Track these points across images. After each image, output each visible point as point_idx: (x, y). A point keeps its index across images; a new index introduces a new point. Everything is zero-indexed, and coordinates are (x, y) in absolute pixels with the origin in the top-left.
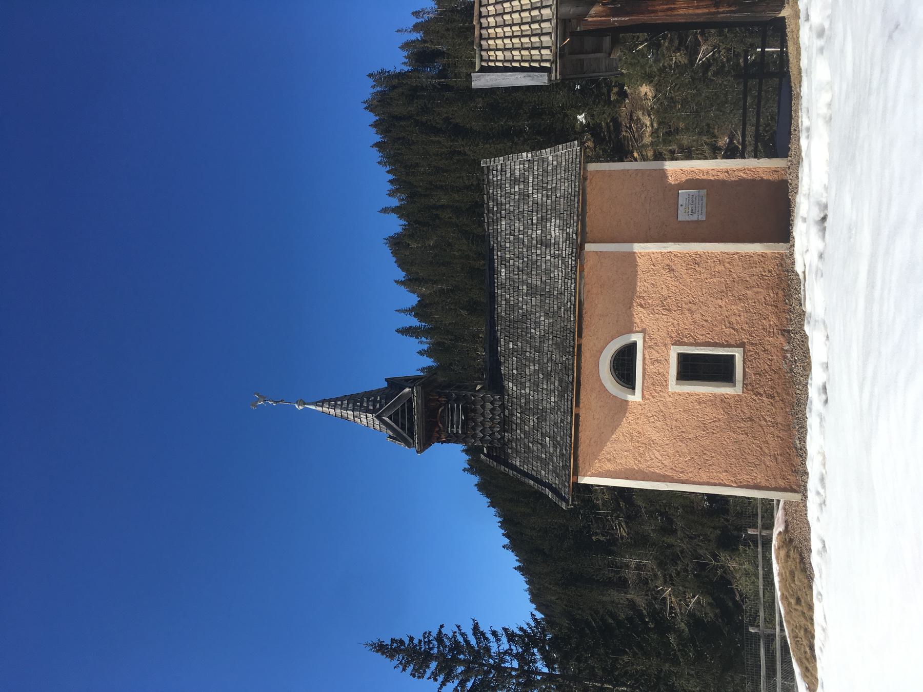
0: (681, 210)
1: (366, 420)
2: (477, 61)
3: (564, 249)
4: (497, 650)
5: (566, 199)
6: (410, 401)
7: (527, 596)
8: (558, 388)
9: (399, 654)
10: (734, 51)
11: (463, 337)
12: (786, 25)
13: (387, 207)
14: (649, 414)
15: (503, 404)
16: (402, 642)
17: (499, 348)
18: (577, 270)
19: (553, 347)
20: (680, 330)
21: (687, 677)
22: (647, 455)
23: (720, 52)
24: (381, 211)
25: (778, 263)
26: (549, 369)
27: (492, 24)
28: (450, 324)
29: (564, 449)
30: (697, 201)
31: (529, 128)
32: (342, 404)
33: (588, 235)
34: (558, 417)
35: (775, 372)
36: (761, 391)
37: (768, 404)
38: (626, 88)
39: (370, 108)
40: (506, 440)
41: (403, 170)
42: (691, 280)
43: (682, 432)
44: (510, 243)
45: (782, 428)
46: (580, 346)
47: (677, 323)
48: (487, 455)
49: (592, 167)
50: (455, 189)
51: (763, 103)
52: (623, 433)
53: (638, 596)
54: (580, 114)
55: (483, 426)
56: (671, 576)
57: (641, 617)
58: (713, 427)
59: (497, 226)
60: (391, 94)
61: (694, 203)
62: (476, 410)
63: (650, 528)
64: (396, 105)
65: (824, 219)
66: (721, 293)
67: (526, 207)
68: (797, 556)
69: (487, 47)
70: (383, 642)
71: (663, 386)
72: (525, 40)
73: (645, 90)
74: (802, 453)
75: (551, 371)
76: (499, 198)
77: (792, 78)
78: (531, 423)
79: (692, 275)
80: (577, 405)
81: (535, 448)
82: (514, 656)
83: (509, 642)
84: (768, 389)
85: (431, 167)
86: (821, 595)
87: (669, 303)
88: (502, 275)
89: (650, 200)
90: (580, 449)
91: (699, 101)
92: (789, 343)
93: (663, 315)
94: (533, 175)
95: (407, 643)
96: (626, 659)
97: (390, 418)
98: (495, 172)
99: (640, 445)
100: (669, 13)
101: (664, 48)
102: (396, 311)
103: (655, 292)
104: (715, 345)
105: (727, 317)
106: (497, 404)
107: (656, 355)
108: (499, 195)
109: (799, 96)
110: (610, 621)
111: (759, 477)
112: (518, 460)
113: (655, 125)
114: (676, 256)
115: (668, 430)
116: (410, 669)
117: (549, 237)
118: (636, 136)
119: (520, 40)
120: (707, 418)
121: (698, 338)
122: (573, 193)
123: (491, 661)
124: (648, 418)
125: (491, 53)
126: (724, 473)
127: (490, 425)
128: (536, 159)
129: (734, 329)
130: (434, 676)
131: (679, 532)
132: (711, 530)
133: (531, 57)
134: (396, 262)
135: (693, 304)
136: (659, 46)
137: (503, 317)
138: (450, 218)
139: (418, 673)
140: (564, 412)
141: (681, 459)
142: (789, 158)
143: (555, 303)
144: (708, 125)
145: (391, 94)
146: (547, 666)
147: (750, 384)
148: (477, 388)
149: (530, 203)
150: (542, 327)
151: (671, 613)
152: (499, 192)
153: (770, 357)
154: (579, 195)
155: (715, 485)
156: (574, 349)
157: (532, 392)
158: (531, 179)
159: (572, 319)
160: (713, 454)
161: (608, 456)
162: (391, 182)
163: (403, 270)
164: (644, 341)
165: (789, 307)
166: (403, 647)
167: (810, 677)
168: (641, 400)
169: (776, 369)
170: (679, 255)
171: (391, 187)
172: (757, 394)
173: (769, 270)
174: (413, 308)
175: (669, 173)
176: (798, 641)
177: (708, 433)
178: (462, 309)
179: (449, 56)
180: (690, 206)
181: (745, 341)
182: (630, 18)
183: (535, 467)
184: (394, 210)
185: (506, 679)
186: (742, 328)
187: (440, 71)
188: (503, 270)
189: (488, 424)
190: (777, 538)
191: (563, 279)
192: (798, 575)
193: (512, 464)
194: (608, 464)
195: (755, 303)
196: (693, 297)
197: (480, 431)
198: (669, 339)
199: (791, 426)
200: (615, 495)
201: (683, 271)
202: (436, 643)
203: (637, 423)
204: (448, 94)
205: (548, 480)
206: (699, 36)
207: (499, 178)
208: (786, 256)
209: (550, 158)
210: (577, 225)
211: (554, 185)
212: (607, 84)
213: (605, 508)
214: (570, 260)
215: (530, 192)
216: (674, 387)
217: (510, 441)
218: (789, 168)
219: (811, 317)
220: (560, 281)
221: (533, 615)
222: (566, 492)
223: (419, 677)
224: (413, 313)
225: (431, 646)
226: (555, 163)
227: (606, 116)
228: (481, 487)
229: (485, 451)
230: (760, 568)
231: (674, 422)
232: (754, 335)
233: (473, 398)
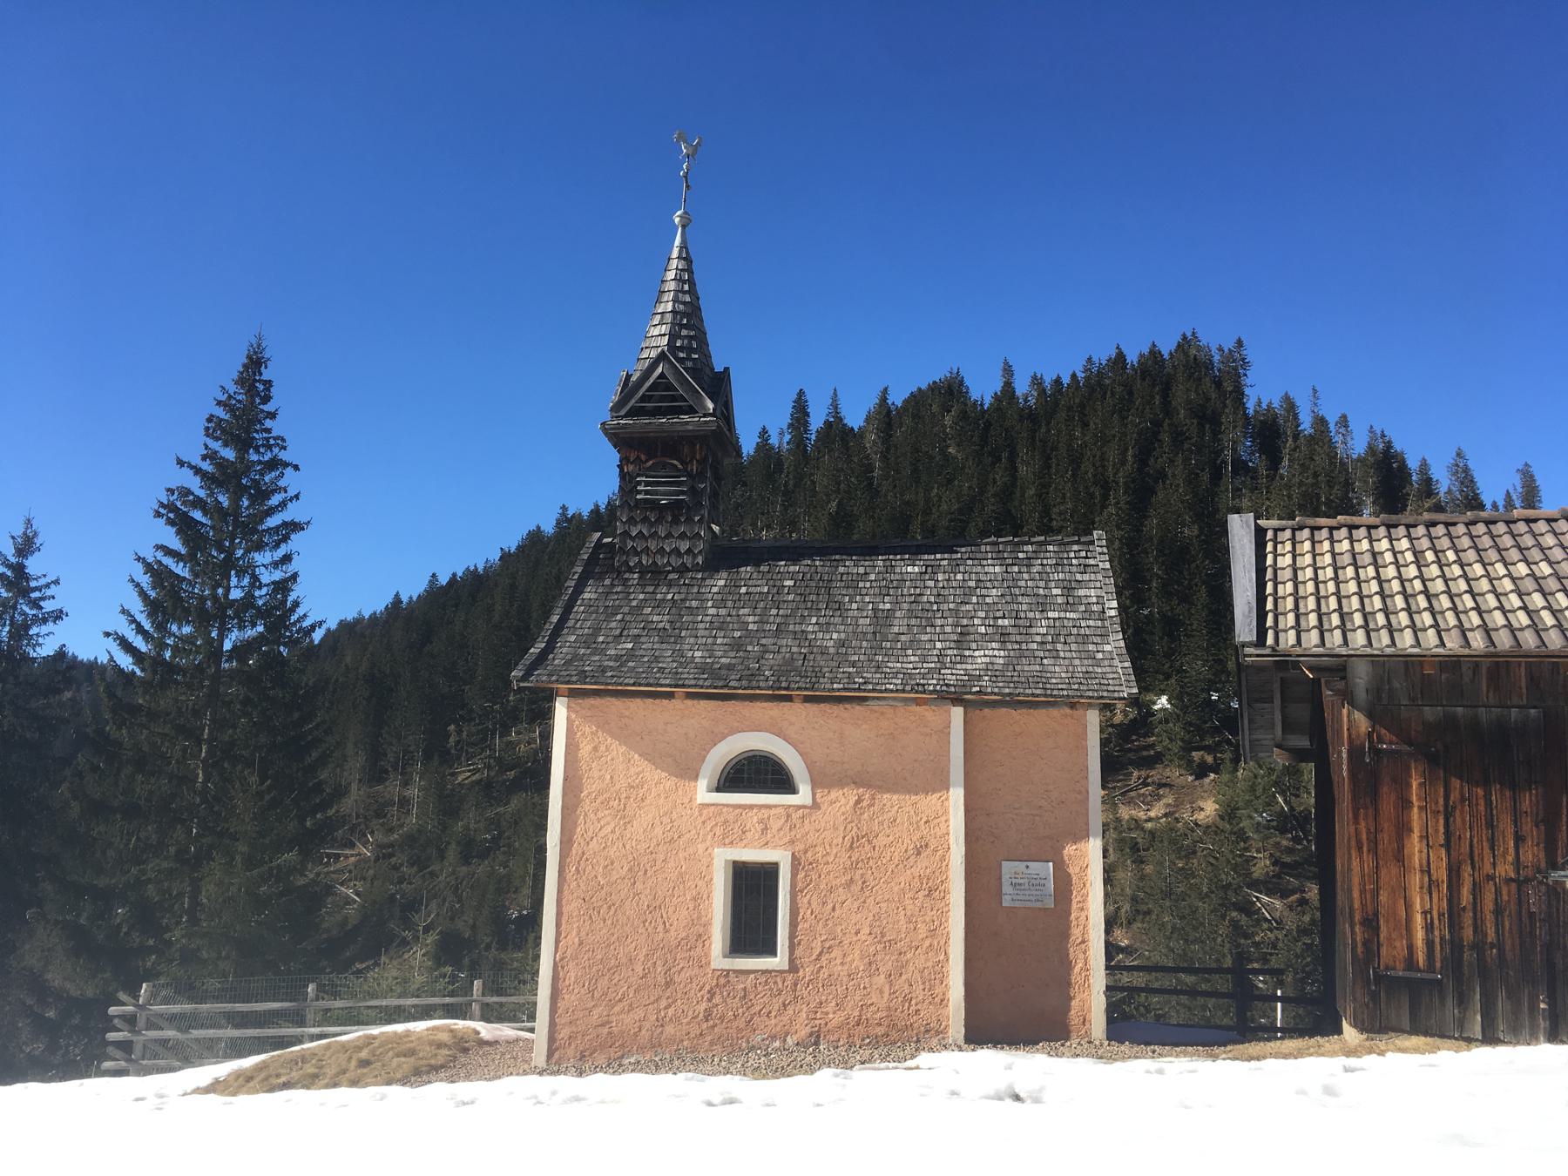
1: (658, 335)
2: (1275, 523)
3: (954, 671)
4: (257, 564)
5: (1039, 674)
6: (691, 411)
7: (350, 616)
8: (718, 663)
9: (246, 394)
10: (1271, 954)
11: (791, 506)
12: (1328, 1036)
14: (674, 816)
15: (688, 570)
17: (783, 563)
18: (918, 693)
19: (788, 655)
21: (226, 881)
22: (607, 812)
23: (1271, 930)
24: (1006, 363)
26: (750, 648)
27: (1338, 548)
28: (813, 482)
29: (614, 673)
30: (1034, 893)
31: (1146, 616)
34: (668, 664)
35: (750, 1022)
36: (718, 999)
38: (1212, 776)
39: (1185, 344)
40: (626, 576)
41: (1077, 401)
43: (646, 871)
44: (964, 580)
46: (789, 699)
48: (599, 544)
49: (1093, 718)
50: (1044, 491)
51: (1184, 999)
53: (356, 801)
54: (1169, 701)
55: (650, 536)
56: (391, 855)
57: (325, 805)
59: (992, 559)
60: (1207, 379)
63: (471, 821)
64: (1188, 389)
65: (1017, 1098)
67: (1025, 607)
68: (440, 1060)
69: (1298, 539)
70: (266, 367)
72: (1311, 603)
73: (1209, 809)
74: (615, 1066)
75: (746, 651)
76: (1039, 561)
77: (1241, 1046)
78: (656, 618)
80: (690, 696)
81: (613, 625)
82: (250, 591)
83: (273, 583)
85: (1082, 449)
86: (381, 1099)
90: (613, 700)
91: (1190, 897)
92: (798, 1044)
93: (844, 838)
95: (266, 408)
96: (254, 779)
97: (662, 375)
98: (1083, 554)
99: (623, 801)
100: (1353, 843)
101: (1278, 839)
103: (881, 823)
104: (793, 924)
106: (688, 560)
108: (1045, 562)
109: (1215, 1057)
110: (315, 754)
111: (573, 998)
112: (593, 596)
113: (1149, 825)
114: (943, 858)
116: (221, 413)
117: (974, 646)
118: (1133, 794)
119: (1311, 594)
122: (1048, 686)
123: (239, 553)
124: (668, 813)
125: (1288, 546)
128: (1107, 624)
129: (820, 954)
130: (210, 456)
131: (464, 869)
132: (471, 921)
133: (1282, 614)
134: (920, 389)
136: (1283, 830)
137: (836, 570)
138: (995, 482)
139: (215, 428)
140: (677, 673)
141: (601, 870)
142: (1106, 1043)
143: (862, 658)
144: (1149, 912)
145: (1207, 379)
146: (235, 648)
147: (729, 981)
148: (713, 526)
149: (1031, 615)
150: (820, 635)
151: (328, 856)
152: (1050, 562)
153: (773, 1014)
154: (1046, 696)
155: (558, 925)
156: (785, 689)
157: (709, 618)
158: (1072, 615)
159: (835, 686)
160: (609, 922)
161: (603, 748)
162: (1058, 381)
163: (906, 401)
165: (858, 1043)
166: (258, 401)
167: (236, 1084)
168: (699, 801)
170: (944, 864)
171: (1048, 381)
172: (712, 994)
174: (841, 419)
175: (1081, 845)
176: (297, 1064)
177: (645, 913)
178: (839, 504)
179: (1271, 478)
180: (1026, 881)
182: (1346, 780)
183: (582, 624)
184: (1008, 386)
185: (209, 578)
187: (1245, 463)
188: (916, 569)
189: (653, 545)
190: (468, 1028)
191: (903, 671)
192: (408, 1063)
193: (585, 586)
194: (589, 748)
195: (864, 988)
197: (641, 531)
199: (659, 1049)
200: (527, 763)
201: (916, 871)
202: (266, 458)
203: (659, 795)
204: (1205, 477)
206: (1297, 896)
208: (943, 1038)
209: (1107, 648)
210: (995, 694)
211: (1062, 654)
212: (1219, 744)
213: (503, 746)
214: (935, 682)
215: (1051, 614)
216: (722, 858)
217: (625, 582)
218: (1090, 1042)
219: (845, 1078)
220: (899, 665)
221: (320, 624)
222: (540, 677)
223: (207, 429)
224: (832, 419)
225: (262, 450)
226: (1100, 656)
227: (1164, 744)
228: (535, 537)
229: (606, 540)
230: (415, 1001)
231: (662, 857)
232: (811, 987)
233: (697, 519)
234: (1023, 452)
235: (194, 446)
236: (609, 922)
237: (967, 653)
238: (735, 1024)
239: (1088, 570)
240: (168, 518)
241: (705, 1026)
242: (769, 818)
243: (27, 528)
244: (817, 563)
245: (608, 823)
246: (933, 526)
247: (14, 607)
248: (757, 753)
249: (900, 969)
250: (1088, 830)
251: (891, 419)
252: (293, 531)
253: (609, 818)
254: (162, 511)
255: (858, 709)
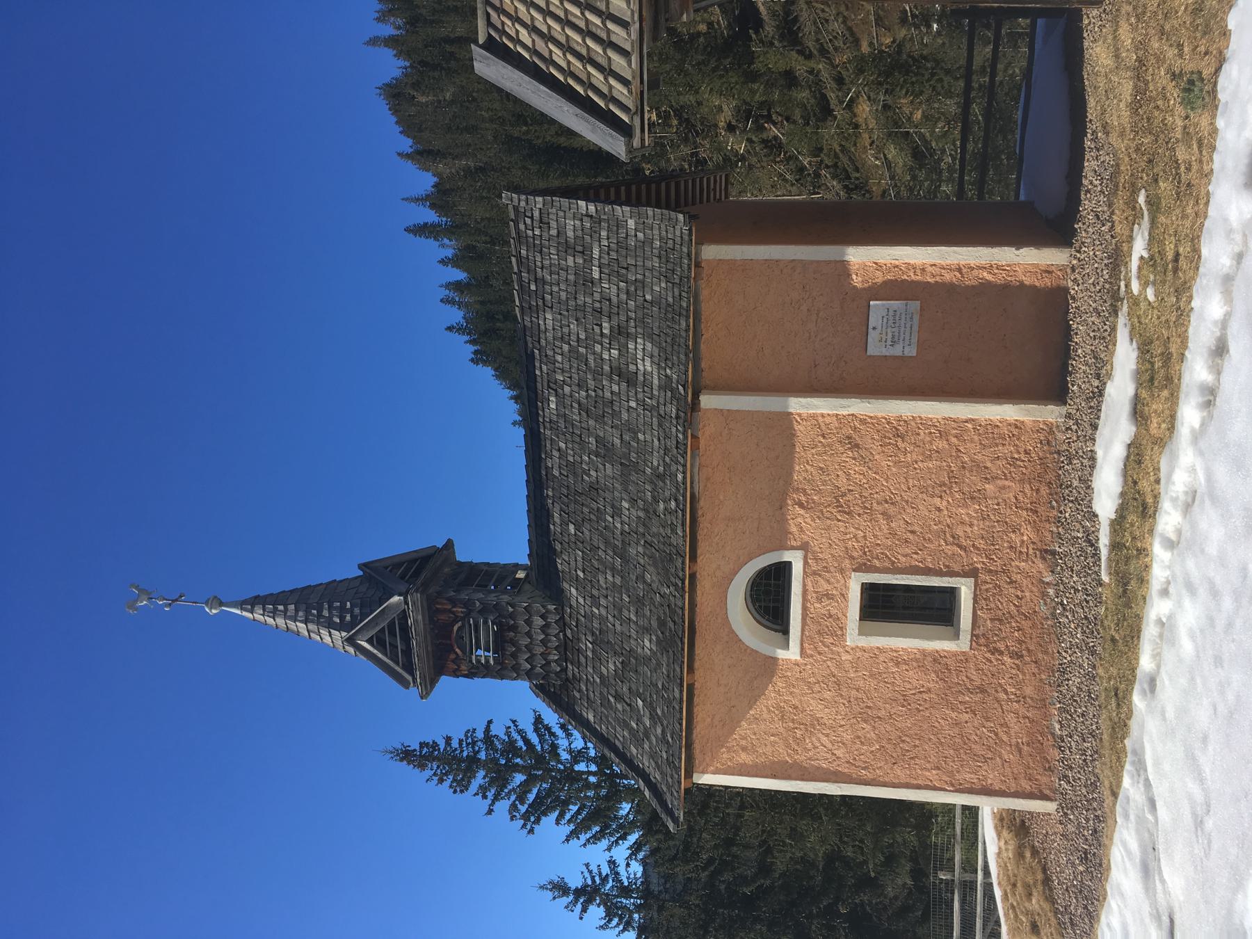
0: (873, 336)
1: (333, 639)
6: (404, 616)
9: (432, 763)
13: (378, 37)
15: (562, 618)
16: (435, 745)
17: (552, 527)
20: (868, 547)
25: (1042, 438)
30: (903, 321)
32: (286, 610)
33: (704, 374)
35: (1026, 616)
36: (1001, 646)
37: (1011, 667)
42: (889, 463)
45: (1032, 704)
46: (693, 577)
47: (862, 534)
49: (711, 252)
52: (767, 707)
58: (919, 700)
61: (897, 325)
62: (518, 627)
66: (941, 486)
70: (409, 746)
71: (836, 636)
76: (539, 270)
79: (891, 456)
80: (691, 669)
84: (1013, 644)
87: (849, 501)
88: (551, 406)
89: (817, 315)
90: (695, 732)
92: (1052, 572)
93: (839, 521)
94: (600, 246)
95: (442, 747)
97: (370, 641)
102: (403, 199)
103: (824, 483)
104: (927, 572)
105: (948, 526)
106: (552, 619)
107: (826, 586)
111: (991, 776)
114: (863, 422)
115: (844, 704)
120: (909, 686)
121: (898, 559)
126: (934, 772)
127: (542, 650)
129: (960, 547)
135: (892, 504)
139: (461, 786)
141: (865, 747)
147: (983, 635)
153: (1019, 593)
155: (918, 787)
160: (917, 742)
161: (743, 743)
164: (806, 563)
168: (798, 658)
169: (1028, 613)
173: (1025, 451)
174: (427, 196)
175: (853, 268)
177: (910, 710)
180: (889, 330)
181: (979, 566)
184: (391, 42)
186: (973, 545)
189: (539, 650)
196: (892, 493)
197: (526, 660)
198: (847, 561)
199: (1048, 701)
201: (876, 448)
203: (791, 693)
205: (643, 764)
207: (537, 232)
216: (854, 636)
223: (462, 791)
224: (428, 203)
226: (640, 235)
231: (854, 692)
232: (994, 557)
233: (511, 609)
234: (444, 32)
235: (471, 802)
236: (917, 742)
237: (641, 378)
238: (1029, 631)
239: (545, 220)
240: (534, 823)
241: (1027, 659)
242: (816, 592)
243: (547, 889)
244: (550, 493)
245: (819, 740)
246: (514, 115)
247: (607, 895)
248: (748, 593)
249: (979, 467)
250: (836, 262)
251: (425, 151)
252: (541, 723)
253: (814, 739)
254: (528, 827)
255: (702, 503)
